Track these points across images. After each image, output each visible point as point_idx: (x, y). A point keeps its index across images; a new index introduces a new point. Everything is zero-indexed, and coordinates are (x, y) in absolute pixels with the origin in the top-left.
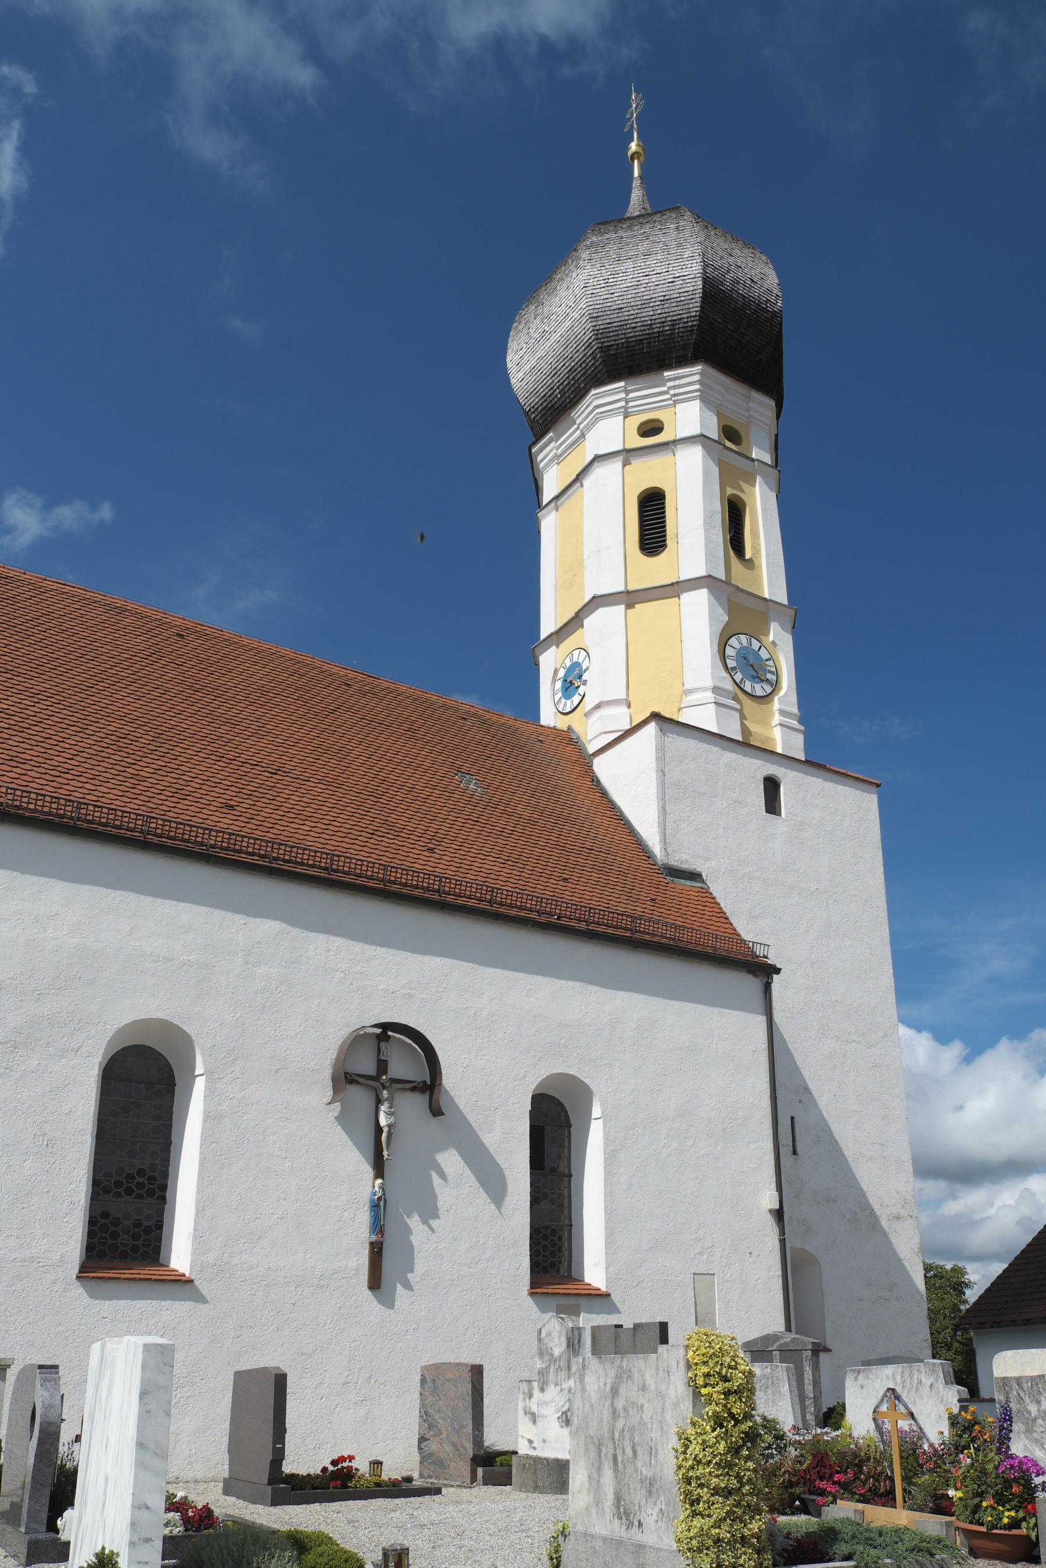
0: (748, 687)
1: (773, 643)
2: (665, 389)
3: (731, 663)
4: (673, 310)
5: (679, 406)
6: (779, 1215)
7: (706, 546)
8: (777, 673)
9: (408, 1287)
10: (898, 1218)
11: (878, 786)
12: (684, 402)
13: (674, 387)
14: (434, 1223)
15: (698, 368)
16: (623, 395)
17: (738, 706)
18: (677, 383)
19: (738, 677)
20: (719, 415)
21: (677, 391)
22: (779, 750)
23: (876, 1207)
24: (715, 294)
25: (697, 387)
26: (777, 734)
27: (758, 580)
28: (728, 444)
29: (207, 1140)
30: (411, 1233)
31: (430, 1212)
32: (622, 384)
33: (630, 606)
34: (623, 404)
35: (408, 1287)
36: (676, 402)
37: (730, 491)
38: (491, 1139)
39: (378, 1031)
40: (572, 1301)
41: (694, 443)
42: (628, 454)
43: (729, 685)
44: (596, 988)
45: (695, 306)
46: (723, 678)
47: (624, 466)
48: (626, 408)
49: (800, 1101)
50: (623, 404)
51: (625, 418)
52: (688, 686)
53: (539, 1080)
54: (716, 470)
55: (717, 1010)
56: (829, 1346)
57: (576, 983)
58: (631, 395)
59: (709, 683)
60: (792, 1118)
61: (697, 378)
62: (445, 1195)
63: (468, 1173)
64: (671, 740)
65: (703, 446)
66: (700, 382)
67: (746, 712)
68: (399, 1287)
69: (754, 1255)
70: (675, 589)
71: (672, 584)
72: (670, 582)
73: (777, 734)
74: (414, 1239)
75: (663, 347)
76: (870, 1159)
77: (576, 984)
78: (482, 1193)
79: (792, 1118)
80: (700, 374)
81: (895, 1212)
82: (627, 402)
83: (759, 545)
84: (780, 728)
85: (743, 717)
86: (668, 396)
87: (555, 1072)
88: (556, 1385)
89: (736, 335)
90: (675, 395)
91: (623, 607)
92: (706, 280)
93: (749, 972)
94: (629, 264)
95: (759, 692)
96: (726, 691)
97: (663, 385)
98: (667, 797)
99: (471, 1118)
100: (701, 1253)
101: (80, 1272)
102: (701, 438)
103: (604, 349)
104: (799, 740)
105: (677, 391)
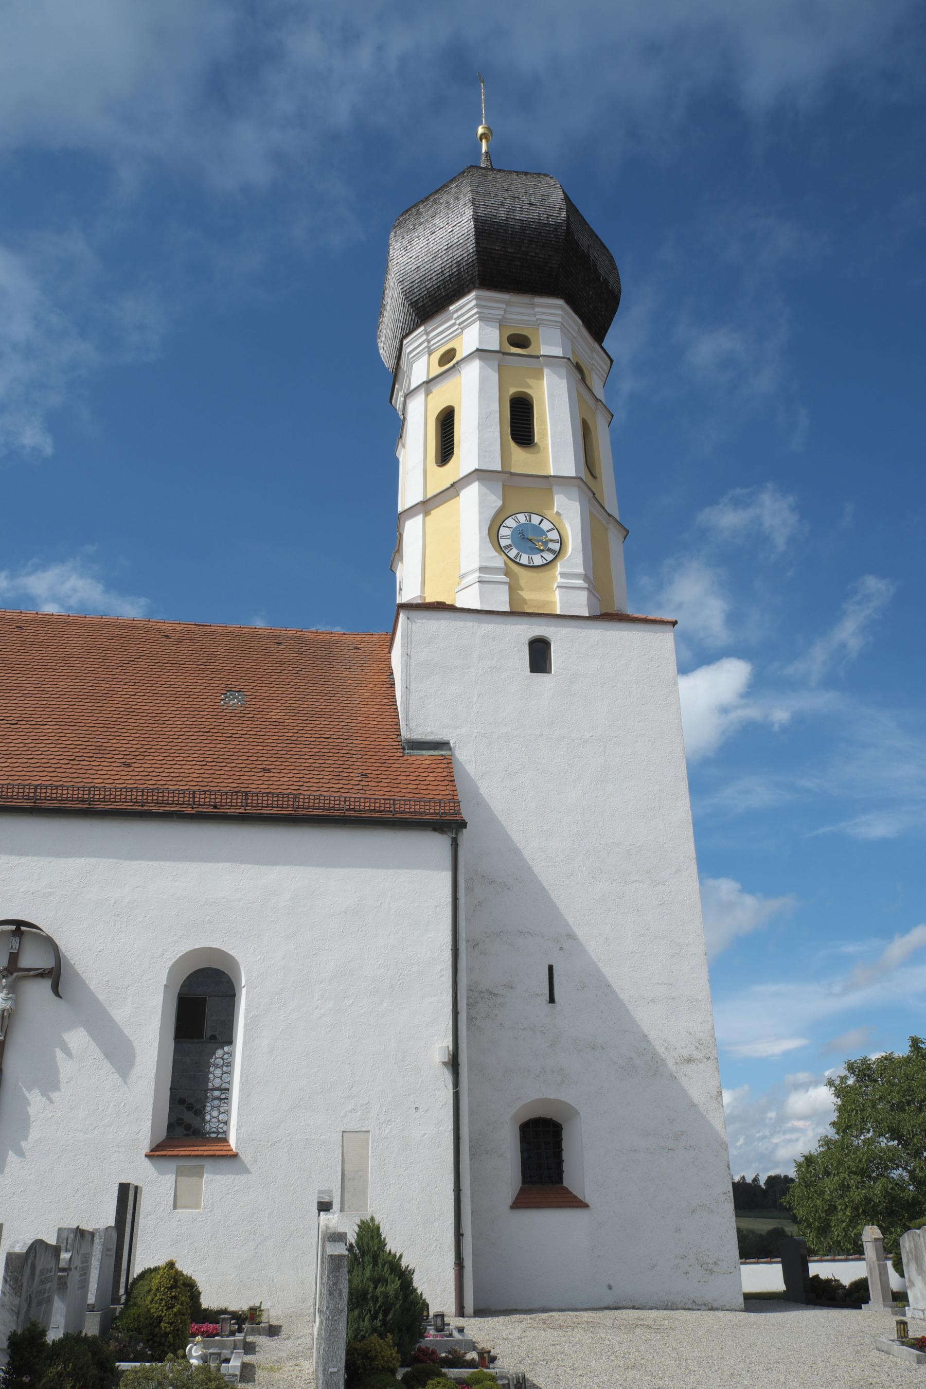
0: (524, 559)
1: (557, 513)
2: (453, 321)
3: (504, 543)
4: (457, 253)
5: (465, 332)
6: (454, 1064)
7: (480, 444)
8: (561, 541)
9: (20, 1153)
10: (689, 1060)
11: (674, 623)
12: (469, 327)
13: (458, 318)
14: (54, 1095)
15: (473, 295)
16: (424, 337)
17: (508, 580)
18: (460, 313)
19: (513, 553)
20: (501, 327)
21: (461, 320)
22: (558, 612)
23: (661, 1050)
24: (486, 230)
25: (475, 310)
26: (557, 596)
27: (544, 463)
28: (514, 350)
29: (246, 1031)
30: (29, 1104)
31: (49, 1083)
32: (422, 328)
33: (427, 513)
34: (425, 344)
35: (20, 1153)
36: (463, 329)
37: (512, 390)
38: (120, 1014)
39: (13, 928)
40: (194, 1162)
41: (472, 358)
42: (429, 383)
43: (498, 561)
44: (249, 866)
45: (471, 245)
46: (492, 557)
47: (427, 395)
48: (428, 347)
49: (561, 949)
50: (425, 344)
51: (430, 355)
52: (462, 572)
53: (178, 956)
54: (495, 376)
55: (391, 872)
56: (588, 1200)
57: (227, 864)
58: (432, 335)
59: (476, 565)
60: (551, 968)
61: (474, 303)
62: (66, 1067)
63: (93, 1045)
64: (418, 625)
65: (480, 359)
66: (477, 306)
68: (11, 1154)
69: (421, 1110)
70: (454, 489)
71: (452, 485)
72: (449, 485)
73: (557, 596)
74: (31, 1111)
76: (653, 1001)
77: (227, 865)
78: (106, 1064)
79: (551, 968)
80: (477, 298)
81: (686, 1055)
82: (429, 342)
83: (546, 429)
84: (562, 588)
85: (513, 589)
87: (197, 947)
88: (351, 1245)
89: (519, 256)
90: (460, 324)
91: (421, 517)
92: (476, 219)
93: (435, 830)
94: (421, 229)
95: (537, 560)
96: (495, 568)
97: (451, 318)
98: (412, 678)
99: (101, 997)
100: (354, 1110)
101: (152, 1151)
102: (480, 352)
103: (414, 305)
104: (583, 596)
105: (461, 320)
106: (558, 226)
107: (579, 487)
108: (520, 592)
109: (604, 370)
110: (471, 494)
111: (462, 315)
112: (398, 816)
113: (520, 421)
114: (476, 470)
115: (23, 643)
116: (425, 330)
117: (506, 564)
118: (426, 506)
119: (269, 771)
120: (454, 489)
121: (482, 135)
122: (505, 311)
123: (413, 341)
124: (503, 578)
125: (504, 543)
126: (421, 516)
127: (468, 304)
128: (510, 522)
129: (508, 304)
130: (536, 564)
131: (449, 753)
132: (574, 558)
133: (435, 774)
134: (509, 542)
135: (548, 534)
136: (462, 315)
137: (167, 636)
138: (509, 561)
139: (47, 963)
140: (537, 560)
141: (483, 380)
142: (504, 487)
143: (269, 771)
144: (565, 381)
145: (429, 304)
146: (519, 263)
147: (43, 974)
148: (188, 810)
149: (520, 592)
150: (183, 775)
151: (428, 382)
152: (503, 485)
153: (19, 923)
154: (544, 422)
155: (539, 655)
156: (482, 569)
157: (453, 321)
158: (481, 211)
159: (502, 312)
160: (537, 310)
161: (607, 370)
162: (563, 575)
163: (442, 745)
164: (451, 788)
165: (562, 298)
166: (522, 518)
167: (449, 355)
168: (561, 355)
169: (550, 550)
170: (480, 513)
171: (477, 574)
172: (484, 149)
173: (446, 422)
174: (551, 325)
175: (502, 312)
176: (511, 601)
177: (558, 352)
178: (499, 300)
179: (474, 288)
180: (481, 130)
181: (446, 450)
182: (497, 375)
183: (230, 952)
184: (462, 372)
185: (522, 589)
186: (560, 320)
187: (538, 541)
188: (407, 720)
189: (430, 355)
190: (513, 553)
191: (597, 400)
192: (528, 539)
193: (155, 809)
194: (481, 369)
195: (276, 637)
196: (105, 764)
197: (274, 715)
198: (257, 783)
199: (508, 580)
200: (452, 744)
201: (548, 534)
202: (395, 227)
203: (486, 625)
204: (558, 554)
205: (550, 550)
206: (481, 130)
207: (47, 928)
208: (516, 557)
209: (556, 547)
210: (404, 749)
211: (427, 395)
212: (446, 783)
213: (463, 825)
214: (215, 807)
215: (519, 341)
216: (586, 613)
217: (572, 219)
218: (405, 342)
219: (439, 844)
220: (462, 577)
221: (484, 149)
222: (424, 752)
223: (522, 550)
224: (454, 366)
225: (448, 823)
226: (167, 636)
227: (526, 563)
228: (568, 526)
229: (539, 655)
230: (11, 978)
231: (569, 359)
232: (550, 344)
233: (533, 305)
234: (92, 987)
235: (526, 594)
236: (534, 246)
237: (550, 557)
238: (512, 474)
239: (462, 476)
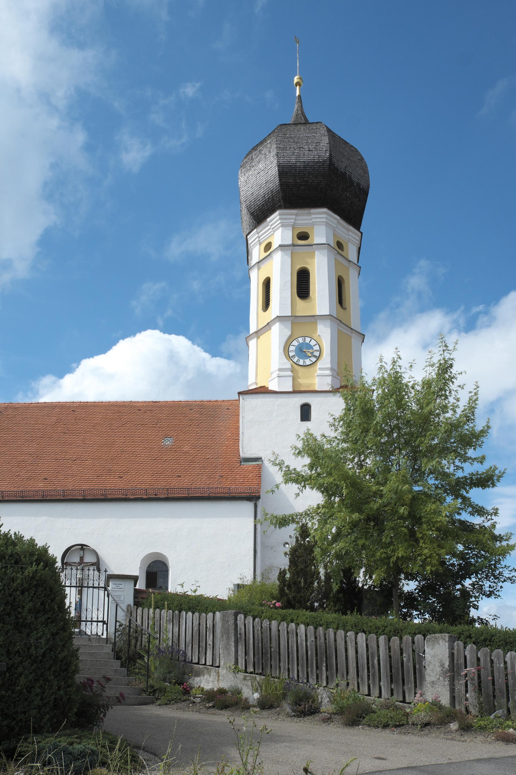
0: (301, 362)
3: (291, 354)
7: (280, 302)
8: (320, 351)
12: (278, 229)
13: (271, 225)
15: (277, 213)
16: (257, 235)
18: (272, 223)
19: (295, 360)
21: (273, 226)
24: (284, 172)
25: (279, 222)
32: (255, 230)
33: (258, 338)
34: (257, 239)
36: (274, 231)
37: (298, 267)
43: (288, 365)
47: (259, 269)
48: (259, 241)
50: (257, 239)
51: (260, 245)
52: (271, 371)
54: (289, 260)
58: (260, 234)
59: (277, 368)
61: (278, 217)
66: (280, 219)
67: (300, 374)
70: (269, 326)
71: (268, 324)
72: (266, 324)
75: (272, 204)
80: (280, 215)
82: (259, 237)
86: (271, 230)
89: (303, 183)
92: (279, 166)
93: (247, 500)
95: (308, 362)
103: (252, 214)
104: (329, 380)
105: (273, 226)
106: (324, 161)
107: (330, 319)
108: (299, 380)
109: (357, 240)
110: (276, 328)
111: (273, 224)
112: (232, 495)
114: (278, 317)
115: (76, 419)
116: (257, 231)
117: (292, 365)
118: (258, 333)
119: (180, 477)
120: (269, 326)
121: (296, 83)
122: (295, 219)
123: (251, 237)
124: (290, 373)
125: (291, 354)
126: (255, 339)
127: (275, 218)
128: (295, 343)
129: (297, 215)
130: (307, 364)
131: (261, 463)
132: (326, 361)
133: (253, 474)
134: (294, 354)
135: (314, 347)
136: (273, 224)
137: (139, 410)
138: (293, 364)
139: (93, 560)
141: (283, 264)
142: (292, 324)
143: (180, 477)
144: (326, 258)
146: (303, 188)
147: (93, 564)
148: (145, 497)
149: (299, 380)
150: (144, 481)
151: (258, 262)
152: (292, 323)
153: (82, 545)
154: (314, 284)
156: (280, 370)
157: (269, 227)
158: (281, 161)
159: (293, 221)
160: (313, 216)
161: (358, 238)
162: (320, 369)
163: (258, 459)
164: (258, 480)
165: (326, 207)
166: (301, 340)
167: (268, 246)
168: (325, 242)
169: (314, 356)
170: (280, 339)
171: (277, 372)
172: (298, 93)
173: (267, 283)
174: (321, 224)
175: (293, 221)
176: (294, 386)
177: (323, 241)
178: (291, 215)
179: (280, 207)
180: (296, 79)
181: (267, 304)
182: (290, 259)
183: (164, 554)
184: (274, 258)
185: (300, 378)
186: (325, 220)
187: (308, 352)
188: (243, 448)
189: (260, 245)
190: (295, 360)
191: (350, 261)
192: (303, 351)
193: (131, 497)
194: (282, 256)
195: (190, 405)
196: (112, 477)
197: (186, 449)
198: (175, 483)
199: (292, 375)
200: (263, 459)
201: (314, 347)
202: (241, 166)
203: (280, 399)
204: (318, 358)
205: (314, 356)
206: (296, 79)
207: (92, 546)
208: (297, 362)
209: (317, 354)
210: (241, 462)
211: (259, 269)
212: (257, 478)
213: (259, 498)
214: (156, 495)
215: (303, 236)
216: (328, 388)
217: (333, 155)
218: (248, 237)
219: (249, 506)
220: (272, 373)
221: (298, 93)
222: (250, 463)
223: (300, 357)
224: (269, 255)
225: (253, 498)
226: (139, 410)
227: (302, 364)
228: (324, 342)
230: (81, 566)
231: (328, 244)
232: (319, 236)
233: (310, 214)
234: (112, 569)
235: (301, 381)
236: (311, 177)
237: (314, 359)
238: (296, 317)
239: (272, 319)
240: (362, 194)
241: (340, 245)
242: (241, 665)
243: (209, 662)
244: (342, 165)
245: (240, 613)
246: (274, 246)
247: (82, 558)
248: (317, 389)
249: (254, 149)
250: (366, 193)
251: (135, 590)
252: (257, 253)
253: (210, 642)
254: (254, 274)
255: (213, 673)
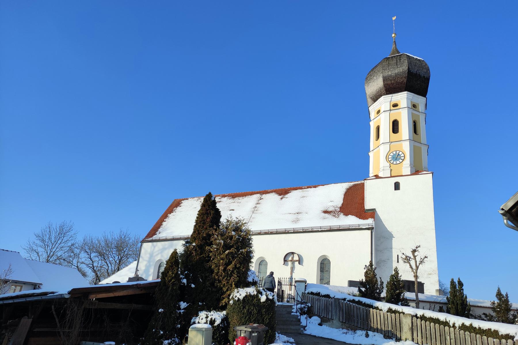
12: (385, 102)
84: (406, 167)
95: (398, 162)
103: (371, 98)
113: (395, 127)
125: (390, 160)
132: (407, 161)
140: (398, 162)
145: (375, 99)
147: (297, 261)
155: (397, 186)
173: (378, 128)
204: (403, 160)
209: (403, 158)
215: (395, 105)
229: (397, 186)
237: (401, 161)
240: (427, 80)
241: (414, 106)
242: (341, 320)
243: (330, 317)
244: (414, 70)
245: (319, 316)
246: (381, 111)
247: (293, 258)
248: (403, 174)
249: (372, 70)
250: (428, 80)
251: (412, 174)
252: (373, 115)
253: (330, 309)
254: (372, 123)
255: (331, 322)
